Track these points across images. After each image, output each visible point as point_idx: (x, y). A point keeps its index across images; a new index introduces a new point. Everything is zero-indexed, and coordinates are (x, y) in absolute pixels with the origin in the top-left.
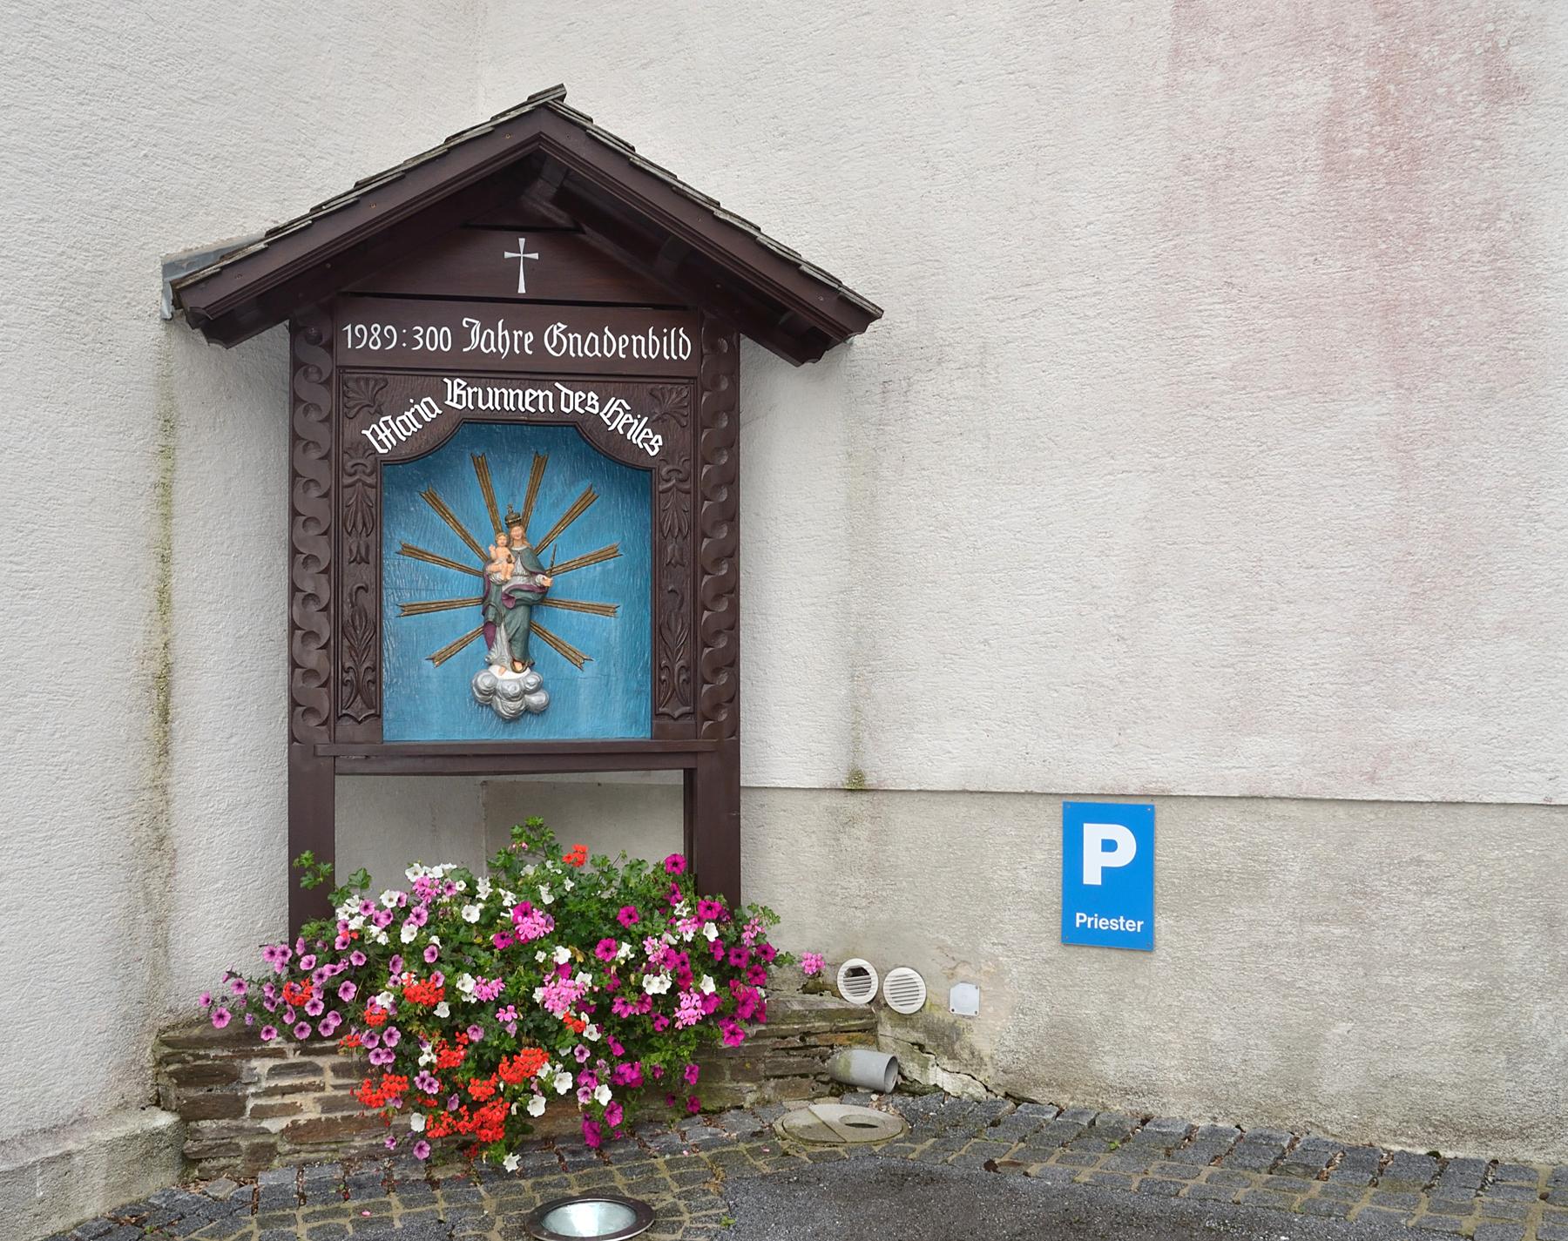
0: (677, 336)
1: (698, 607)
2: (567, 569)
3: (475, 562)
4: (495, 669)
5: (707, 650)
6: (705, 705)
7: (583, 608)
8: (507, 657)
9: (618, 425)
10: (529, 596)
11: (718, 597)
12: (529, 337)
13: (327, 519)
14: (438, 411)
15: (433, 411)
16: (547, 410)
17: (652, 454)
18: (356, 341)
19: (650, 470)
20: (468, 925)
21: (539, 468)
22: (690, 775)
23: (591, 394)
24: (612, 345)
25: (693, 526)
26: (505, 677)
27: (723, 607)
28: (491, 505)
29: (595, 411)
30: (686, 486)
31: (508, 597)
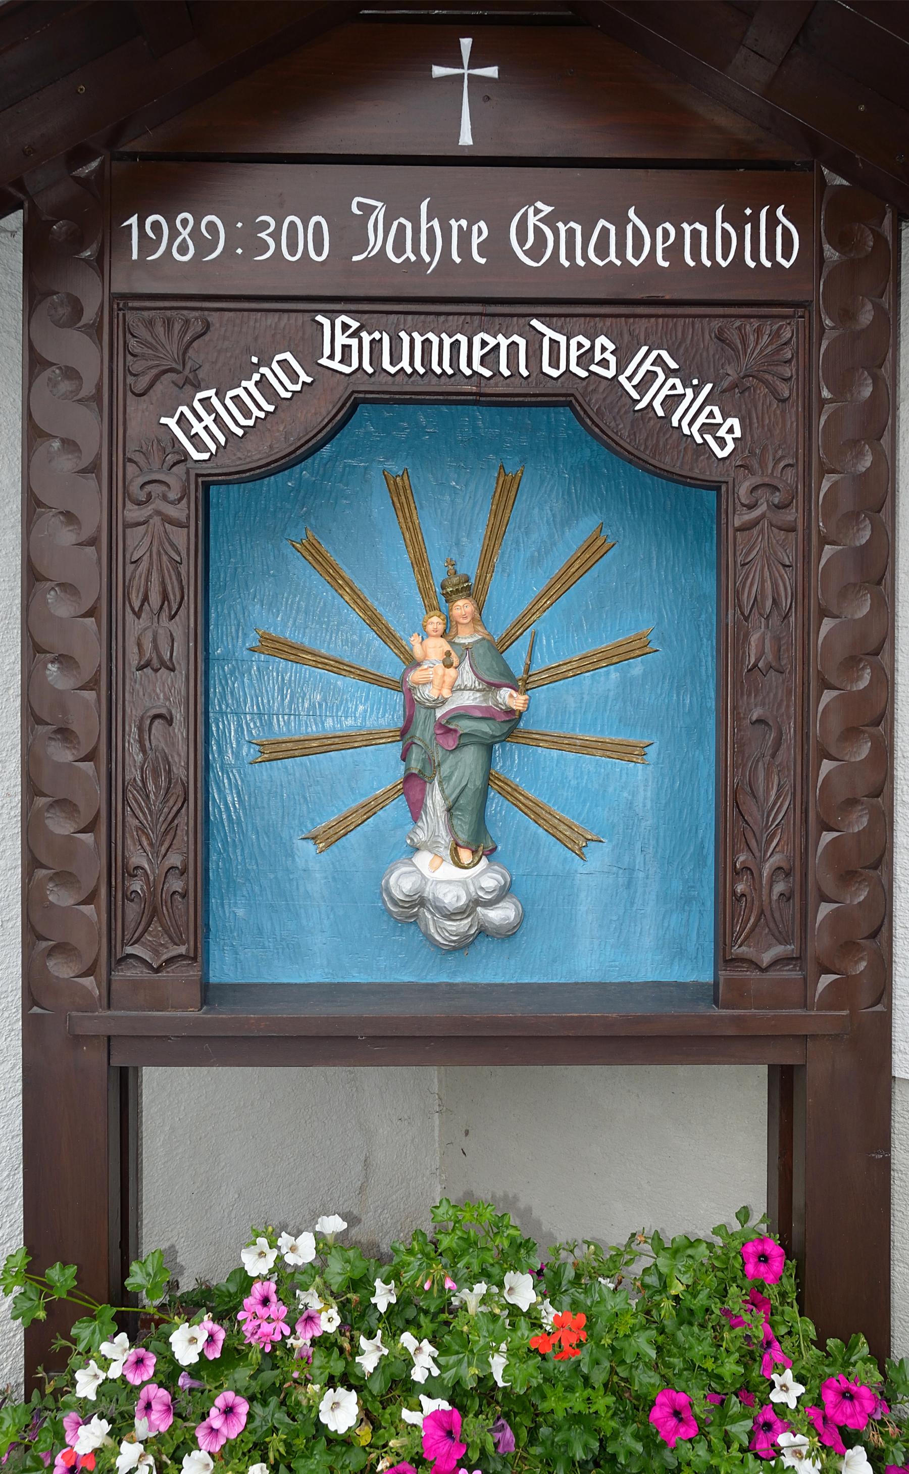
0: (773, 221)
1: (812, 751)
2: (555, 675)
3: (391, 666)
4: (423, 860)
5: (827, 837)
6: (820, 942)
7: (586, 748)
8: (445, 838)
9: (654, 399)
10: (484, 727)
11: (851, 733)
12: (481, 232)
13: (92, 590)
14: (304, 378)
15: (293, 377)
16: (515, 373)
17: (721, 454)
18: (148, 246)
19: (715, 486)
20: (320, 1427)
21: (506, 494)
22: (784, 1086)
23: (602, 340)
24: (642, 242)
25: (802, 593)
26: (440, 875)
27: (864, 750)
28: (420, 563)
29: (610, 374)
30: (790, 516)
31: (445, 729)
